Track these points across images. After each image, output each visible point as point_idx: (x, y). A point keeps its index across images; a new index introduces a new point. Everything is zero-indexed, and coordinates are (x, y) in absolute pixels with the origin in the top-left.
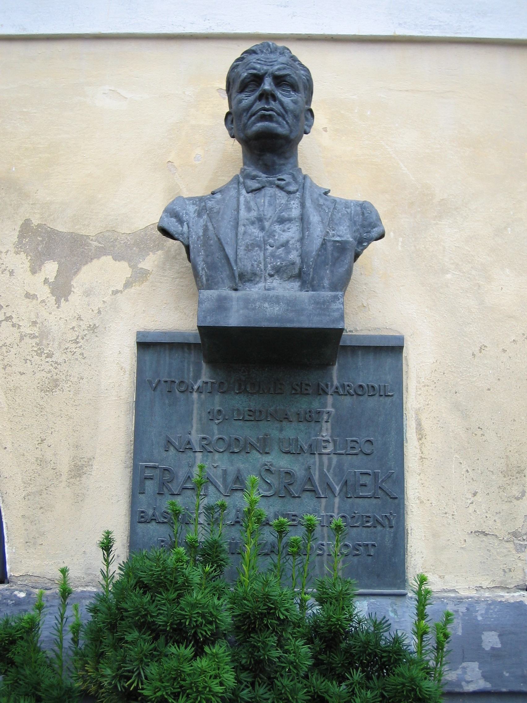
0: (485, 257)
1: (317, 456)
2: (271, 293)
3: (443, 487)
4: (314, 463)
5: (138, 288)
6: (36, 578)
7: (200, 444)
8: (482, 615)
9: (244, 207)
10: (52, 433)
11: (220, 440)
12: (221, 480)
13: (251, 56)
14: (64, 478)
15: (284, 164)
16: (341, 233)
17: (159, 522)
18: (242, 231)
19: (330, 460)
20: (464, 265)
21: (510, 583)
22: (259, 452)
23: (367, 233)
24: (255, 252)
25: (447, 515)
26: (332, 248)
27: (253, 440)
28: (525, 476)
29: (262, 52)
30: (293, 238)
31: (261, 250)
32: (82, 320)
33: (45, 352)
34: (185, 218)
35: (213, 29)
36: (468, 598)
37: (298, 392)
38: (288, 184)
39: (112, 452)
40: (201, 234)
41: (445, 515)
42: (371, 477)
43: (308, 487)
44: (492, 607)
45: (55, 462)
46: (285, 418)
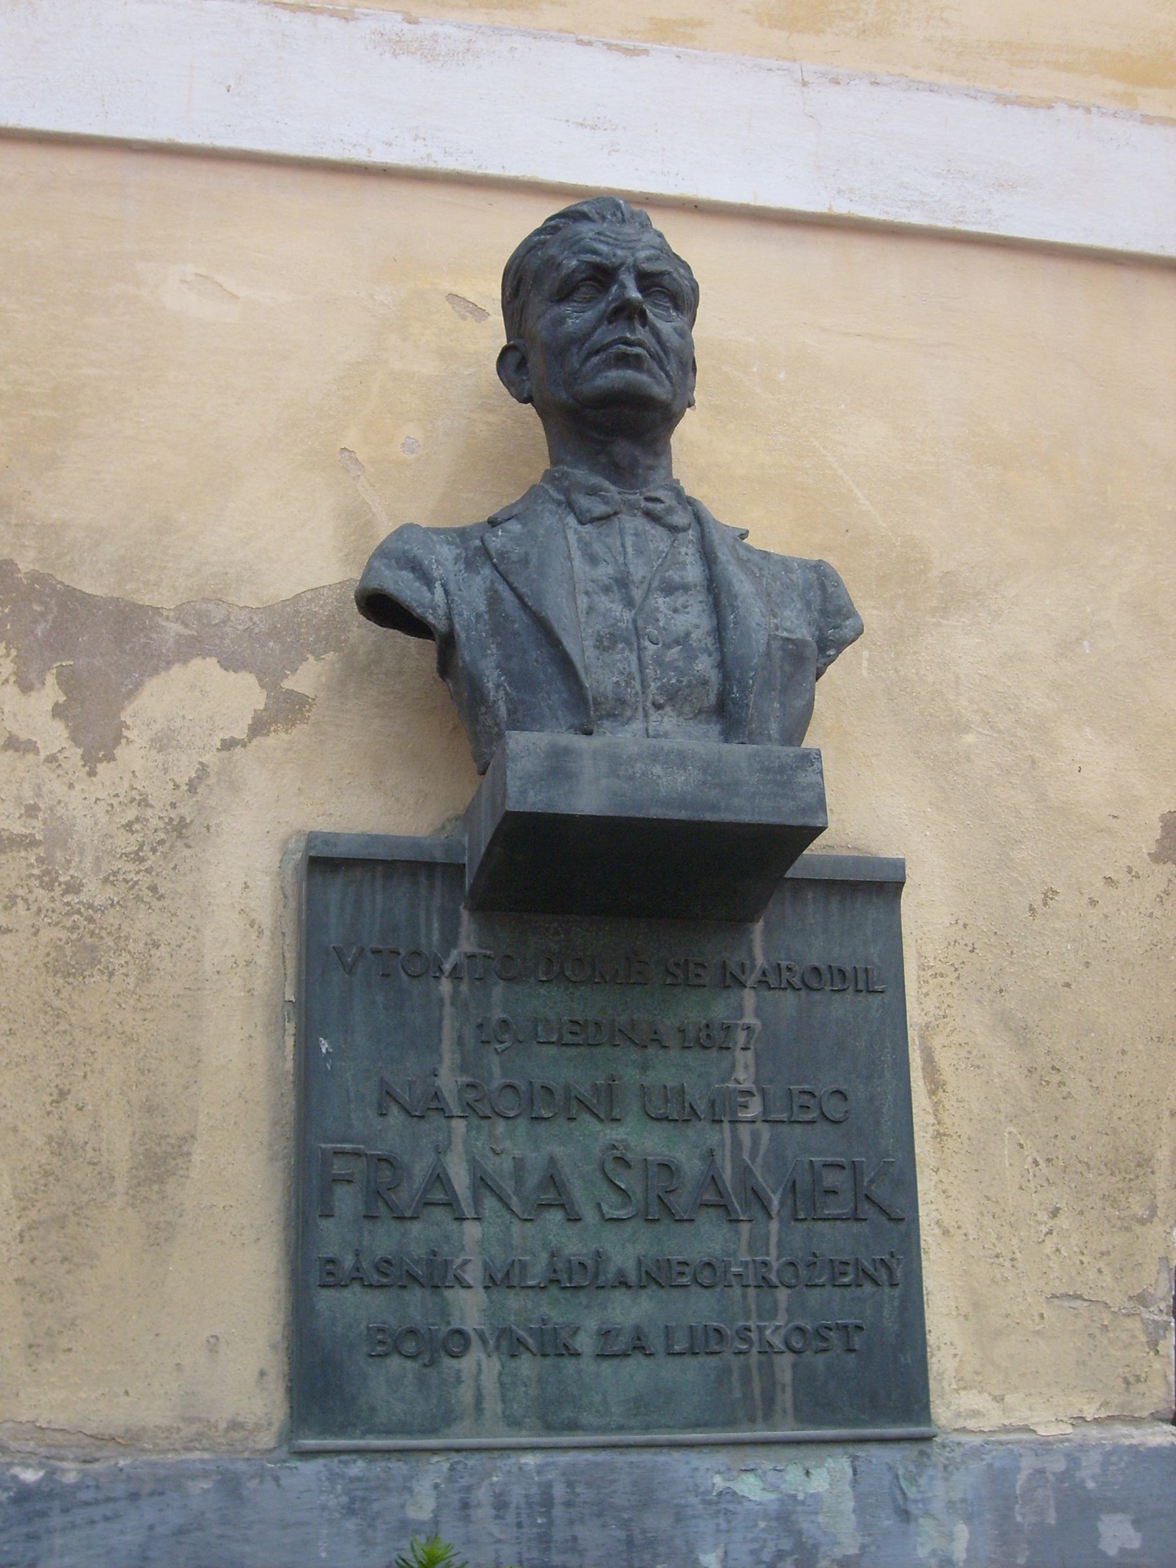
0: (1041, 700)
1: (726, 1126)
2: (666, 744)
3: (988, 1198)
4: (722, 1142)
5: (282, 735)
6: (58, 1436)
7: (460, 1099)
8: (1093, 1477)
9: (579, 553)
10: (85, 1077)
11: (508, 1090)
12: (512, 1183)
13: (578, 224)
14: (120, 1185)
15: (651, 468)
16: (789, 624)
17: (371, 1286)
18: (585, 606)
19: (755, 1137)
20: (1000, 715)
21: (1142, 1408)
22: (597, 1116)
23: (834, 628)
24: (618, 653)
25: (1001, 1259)
26: (780, 653)
27: (584, 1090)
28: (1153, 1173)
29: (604, 218)
30: (697, 627)
31: (631, 650)
32: (152, 806)
33: (62, 879)
34: (437, 572)
35: (435, 162)
36: (1062, 1442)
37: (680, 981)
38: (670, 510)
39: (236, 1123)
40: (482, 608)
41: (997, 1261)
42: (845, 1172)
43: (710, 1196)
44: (1114, 1459)
45: (96, 1146)
46: (652, 1040)
